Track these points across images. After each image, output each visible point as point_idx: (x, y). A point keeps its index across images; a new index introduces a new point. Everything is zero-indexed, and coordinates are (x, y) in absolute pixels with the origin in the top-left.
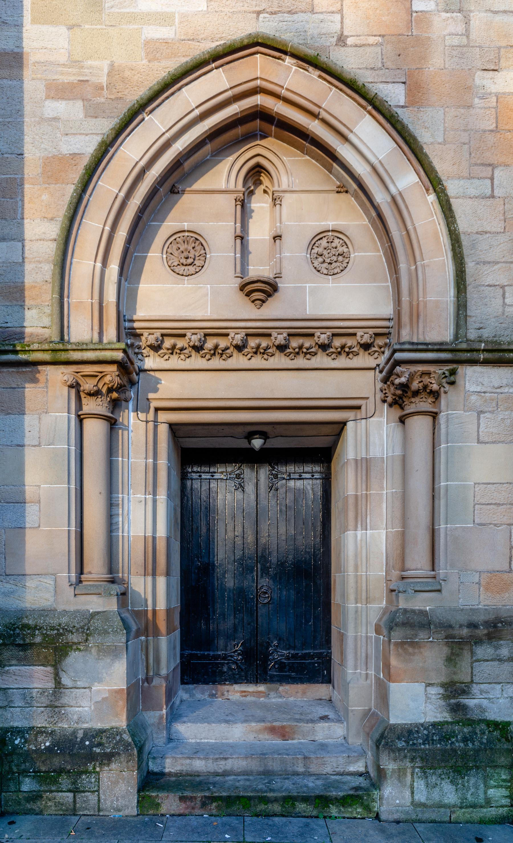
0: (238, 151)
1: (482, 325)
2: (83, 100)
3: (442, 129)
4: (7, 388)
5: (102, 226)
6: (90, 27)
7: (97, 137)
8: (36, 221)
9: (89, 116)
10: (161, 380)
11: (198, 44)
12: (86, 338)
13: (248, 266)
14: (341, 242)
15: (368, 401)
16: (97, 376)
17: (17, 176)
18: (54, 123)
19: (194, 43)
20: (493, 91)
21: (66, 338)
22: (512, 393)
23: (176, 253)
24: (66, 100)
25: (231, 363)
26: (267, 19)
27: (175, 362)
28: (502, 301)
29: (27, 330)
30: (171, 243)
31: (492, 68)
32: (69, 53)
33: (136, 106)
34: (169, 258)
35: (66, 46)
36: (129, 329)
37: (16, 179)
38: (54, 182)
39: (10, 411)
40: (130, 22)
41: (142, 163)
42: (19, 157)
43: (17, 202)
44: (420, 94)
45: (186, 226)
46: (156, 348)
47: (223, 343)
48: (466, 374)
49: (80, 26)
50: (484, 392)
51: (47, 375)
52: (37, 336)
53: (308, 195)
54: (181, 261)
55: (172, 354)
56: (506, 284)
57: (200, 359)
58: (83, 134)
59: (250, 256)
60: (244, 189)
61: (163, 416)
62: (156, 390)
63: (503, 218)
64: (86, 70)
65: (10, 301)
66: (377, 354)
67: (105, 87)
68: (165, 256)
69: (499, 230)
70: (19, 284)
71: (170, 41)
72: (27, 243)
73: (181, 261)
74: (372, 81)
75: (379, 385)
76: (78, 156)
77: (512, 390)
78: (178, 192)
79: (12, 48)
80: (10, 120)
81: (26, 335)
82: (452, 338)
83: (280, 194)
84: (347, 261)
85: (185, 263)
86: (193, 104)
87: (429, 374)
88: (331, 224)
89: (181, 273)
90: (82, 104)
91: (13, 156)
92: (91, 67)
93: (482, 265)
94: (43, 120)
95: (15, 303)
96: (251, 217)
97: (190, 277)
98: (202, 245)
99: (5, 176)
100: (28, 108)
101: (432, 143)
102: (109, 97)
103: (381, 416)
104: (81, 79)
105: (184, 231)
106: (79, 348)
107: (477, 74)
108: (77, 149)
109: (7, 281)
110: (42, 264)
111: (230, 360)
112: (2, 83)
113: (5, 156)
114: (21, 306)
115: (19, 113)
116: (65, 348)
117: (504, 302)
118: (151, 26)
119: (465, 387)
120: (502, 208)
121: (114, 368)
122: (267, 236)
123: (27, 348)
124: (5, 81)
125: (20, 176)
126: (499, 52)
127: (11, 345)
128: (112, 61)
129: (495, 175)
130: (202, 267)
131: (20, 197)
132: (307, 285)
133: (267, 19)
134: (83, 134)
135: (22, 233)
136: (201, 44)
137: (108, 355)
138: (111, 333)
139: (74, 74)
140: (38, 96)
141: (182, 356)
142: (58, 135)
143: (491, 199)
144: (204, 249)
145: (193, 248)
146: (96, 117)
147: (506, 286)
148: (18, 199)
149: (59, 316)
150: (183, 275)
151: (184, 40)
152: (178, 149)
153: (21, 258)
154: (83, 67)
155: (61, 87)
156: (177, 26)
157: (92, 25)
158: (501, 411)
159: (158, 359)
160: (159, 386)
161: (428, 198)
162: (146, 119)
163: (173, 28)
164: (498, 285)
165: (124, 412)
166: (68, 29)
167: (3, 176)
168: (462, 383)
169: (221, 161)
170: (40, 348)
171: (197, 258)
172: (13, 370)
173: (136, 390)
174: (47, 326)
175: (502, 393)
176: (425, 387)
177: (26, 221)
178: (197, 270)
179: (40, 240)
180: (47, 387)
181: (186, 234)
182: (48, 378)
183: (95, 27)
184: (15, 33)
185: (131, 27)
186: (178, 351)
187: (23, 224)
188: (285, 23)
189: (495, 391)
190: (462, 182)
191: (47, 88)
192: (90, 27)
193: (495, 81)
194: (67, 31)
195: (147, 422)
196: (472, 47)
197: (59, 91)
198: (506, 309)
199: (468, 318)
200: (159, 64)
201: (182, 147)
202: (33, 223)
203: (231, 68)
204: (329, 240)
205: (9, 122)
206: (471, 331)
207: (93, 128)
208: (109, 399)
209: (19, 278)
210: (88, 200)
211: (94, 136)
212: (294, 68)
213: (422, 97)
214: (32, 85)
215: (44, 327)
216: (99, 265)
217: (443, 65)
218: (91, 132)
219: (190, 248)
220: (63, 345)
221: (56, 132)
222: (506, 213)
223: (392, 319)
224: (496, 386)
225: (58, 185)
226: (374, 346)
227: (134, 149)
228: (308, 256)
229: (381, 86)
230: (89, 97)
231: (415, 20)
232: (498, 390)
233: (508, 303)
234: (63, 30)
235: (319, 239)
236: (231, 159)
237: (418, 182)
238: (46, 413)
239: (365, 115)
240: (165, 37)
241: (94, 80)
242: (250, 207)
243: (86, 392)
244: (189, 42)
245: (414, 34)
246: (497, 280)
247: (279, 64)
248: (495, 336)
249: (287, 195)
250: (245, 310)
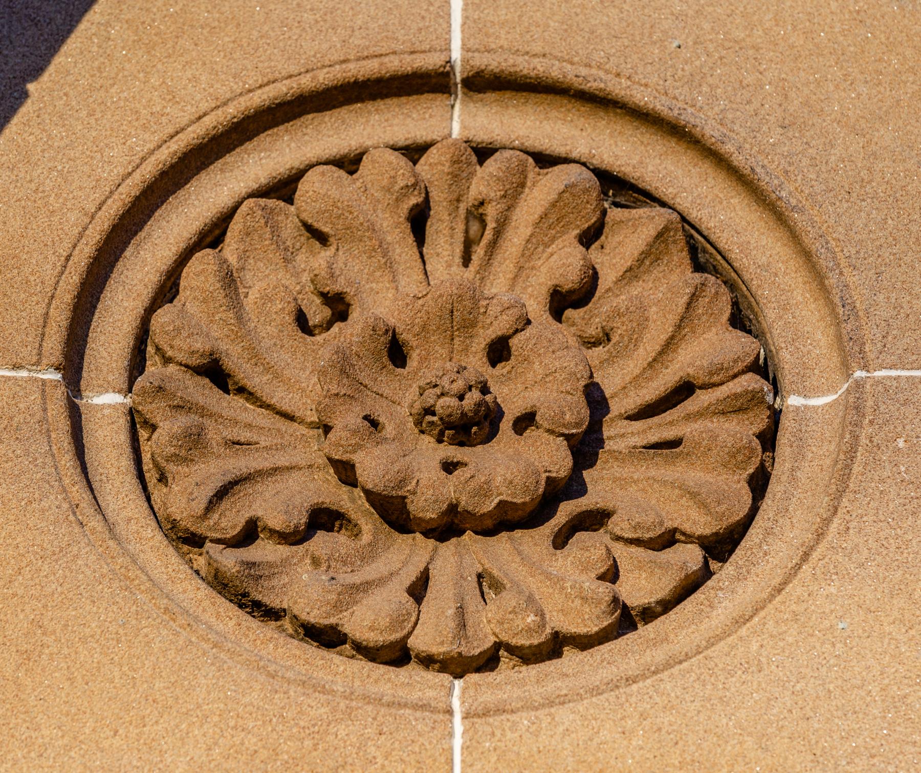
23: (297, 373)
30: (212, 236)
34: (169, 427)
54: (373, 467)
68: (105, 400)
73: (373, 467)
85: (429, 494)
89: (366, 621)
97: (510, 679)
105: (431, 83)
130: (721, 546)
144: (741, 319)
145: (562, 302)
150: (397, 655)
171: (620, 435)
178: (641, 585)
181: (460, 120)
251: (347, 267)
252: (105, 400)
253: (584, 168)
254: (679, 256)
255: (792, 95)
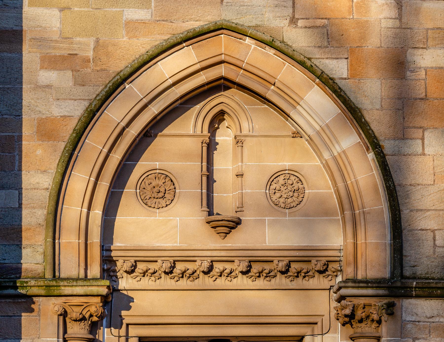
0: (204, 100)
1: (416, 264)
2: (72, 71)
3: (380, 97)
4: (4, 316)
5: (88, 178)
6: (79, 9)
7: (84, 102)
8: (31, 172)
9: (78, 84)
10: (133, 299)
11: (171, 24)
12: (73, 273)
13: (213, 193)
14: (297, 179)
15: (324, 318)
16: (83, 305)
17: (15, 134)
18: (47, 90)
19: (167, 23)
20: (422, 66)
21: (57, 274)
22: (442, 322)
24: (57, 70)
25: (197, 284)
26: (230, 4)
27: (146, 282)
28: (432, 243)
29: (24, 266)
31: (421, 46)
32: (61, 31)
33: (119, 81)
35: (58, 25)
36: (106, 257)
37: (13, 136)
38: (47, 140)
39: (7, 336)
40: (113, 6)
41: (123, 124)
42: (17, 117)
43: (14, 156)
44: (361, 68)
45: (157, 165)
46: (130, 272)
47: (191, 267)
48: (402, 306)
49: (70, 9)
50: (419, 322)
51: (40, 305)
52: (31, 271)
53: (267, 139)
55: (144, 276)
56: (436, 228)
57: (168, 280)
58: (73, 99)
59: (215, 184)
60: (209, 134)
61: (133, 331)
62: (129, 308)
63: (432, 172)
64: (75, 46)
65: (8, 241)
66: (330, 277)
67: (91, 60)
68: (138, 191)
69: (430, 182)
70: (16, 227)
71: (147, 22)
72: (24, 192)
74: (320, 57)
75: (334, 304)
76: (68, 118)
77: (442, 320)
78: (151, 136)
79: (11, 26)
80: (9, 86)
81: (23, 270)
82: (389, 275)
83: (242, 138)
84: (302, 196)
85: (156, 197)
86: (167, 75)
87: (370, 305)
88: (287, 164)
90: (71, 73)
91: (12, 117)
92: (80, 43)
93: (415, 212)
94: (38, 87)
95: (12, 242)
96: (216, 149)
98: (172, 181)
99: (4, 134)
100: (25, 76)
101: (371, 109)
102: (95, 68)
103: (336, 332)
104: (71, 53)
105: (286, 170)
106: (70, 285)
107: (409, 51)
108: (67, 111)
109: (6, 224)
110: (36, 210)
111: (196, 281)
112: (3, 55)
113: (5, 116)
114: (18, 245)
115: (19, 80)
116: (58, 284)
117: (434, 244)
118: (131, 9)
119: (402, 317)
120: (431, 164)
121: (98, 299)
122: (231, 177)
123: (25, 285)
124: (5, 54)
125: (17, 134)
126: (427, 33)
127: (11, 281)
128: (97, 38)
129: (426, 136)
131: (17, 152)
132: (267, 218)
133: (230, 4)
134: (73, 99)
135: (20, 182)
136: (173, 24)
137: (95, 290)
138: (95, 270)
139: (65, 49)
140: (34, 67)
141: (153, 278)
142: (51, 100)
143: (422, 156)
144: (174, 184)
146: (83, 85)
147: (436, 230)
148: (16, 154)
149: (52, 256)
151: (159, 21)
152: (154, 112)
153: (18, 204)
154: (72, 43)
155: (53, 59)
156: (153, 9)
157: (80, 7)
158: (433, 337)
159: (130, 280)
160: (131, 304)
161: (368, 155)
162: (127, 87)
163: (150, 10)
164: (430, 229)
165: (100, 329)
166: (60, 11)
167: (2, 134)
168: (399, 313)
169: (189, 109)
170: (36, 285)
171: (167, 192)
172: (10, 300)
173: (110, 307)
174: (40, 263)
175: (433, 322)
176: (368, 317)
177: (23, 172)
178: (168, 203)
179: (35, 189)
180: (39, 316)
182: (41, 307)
183: (83, 9)
184: (15, 14)
185: (114, 10)
186: (150, 275)
187: (21, 175)
188: (245, 7)
189: (427, 320)
190: (397, 142)
191: (41, 60)
192: (79, 9)
193: (424, 57)
194: (59, 13)
195: (119, 337)
196: (404, 28)
197: (52, 62)
198: (436, 250)
199: (404, 258)
200: (138, 41)
201: (157, 111)
202: (29, 174)
203: (199, 46)
204: (285, 178)
205: (8, 88)
206: (407, 268)
207: (81, 94)
208: (90, 322)
209: (16, 221)
210: (77, 156)
211: (82, 101)
212: (253, 46)
213: (362, 71)
214: (30, 56)
215: (37, 264)
216: (85, 210)
217: (379, 44)
218: (79, 98)
219: (161, 183)
220: (57, 282)
221: (48, 97)
222: (435, 169)
223: (342, 250)
224: (428, 316)
225: (51, 142)
226: (327, 271)
227: (116, 113)
228: (267, 191)
229: (327, 61)
230: (78, 68)
231: (356, 6)
232: (431, 320)
233: (438, 245)
234: (56, 12)
235: (277, 177)
236: (198, 107)
237: (360, 142)
238: (39, 338)
239: (314, 86)
240: (143, 18)
241: (82, 54)
242: (215, 140)
243: (73, 319)
244: (163, 22)
245: (355, 18)
246: (428, 225)
247: (241, 43)
248: (427, 273)
249: (248, 139)
250: (209, 243)
251: (152, 181)
252: (138, 191)
253: (271, 52)
254: (170, 181)
255: (296, 188)
